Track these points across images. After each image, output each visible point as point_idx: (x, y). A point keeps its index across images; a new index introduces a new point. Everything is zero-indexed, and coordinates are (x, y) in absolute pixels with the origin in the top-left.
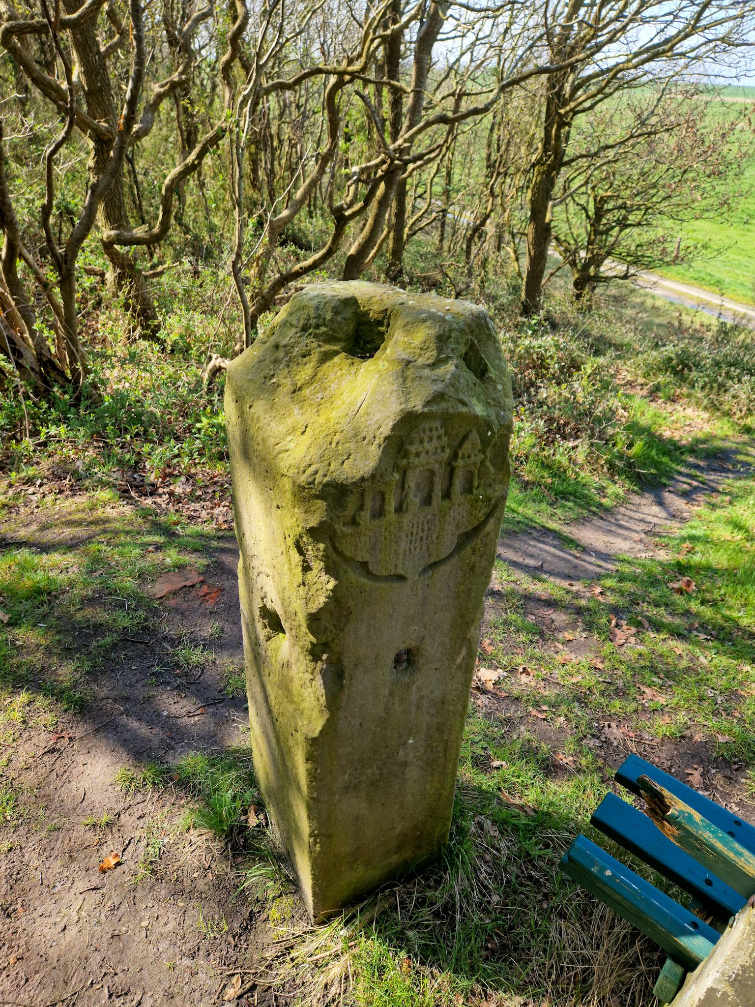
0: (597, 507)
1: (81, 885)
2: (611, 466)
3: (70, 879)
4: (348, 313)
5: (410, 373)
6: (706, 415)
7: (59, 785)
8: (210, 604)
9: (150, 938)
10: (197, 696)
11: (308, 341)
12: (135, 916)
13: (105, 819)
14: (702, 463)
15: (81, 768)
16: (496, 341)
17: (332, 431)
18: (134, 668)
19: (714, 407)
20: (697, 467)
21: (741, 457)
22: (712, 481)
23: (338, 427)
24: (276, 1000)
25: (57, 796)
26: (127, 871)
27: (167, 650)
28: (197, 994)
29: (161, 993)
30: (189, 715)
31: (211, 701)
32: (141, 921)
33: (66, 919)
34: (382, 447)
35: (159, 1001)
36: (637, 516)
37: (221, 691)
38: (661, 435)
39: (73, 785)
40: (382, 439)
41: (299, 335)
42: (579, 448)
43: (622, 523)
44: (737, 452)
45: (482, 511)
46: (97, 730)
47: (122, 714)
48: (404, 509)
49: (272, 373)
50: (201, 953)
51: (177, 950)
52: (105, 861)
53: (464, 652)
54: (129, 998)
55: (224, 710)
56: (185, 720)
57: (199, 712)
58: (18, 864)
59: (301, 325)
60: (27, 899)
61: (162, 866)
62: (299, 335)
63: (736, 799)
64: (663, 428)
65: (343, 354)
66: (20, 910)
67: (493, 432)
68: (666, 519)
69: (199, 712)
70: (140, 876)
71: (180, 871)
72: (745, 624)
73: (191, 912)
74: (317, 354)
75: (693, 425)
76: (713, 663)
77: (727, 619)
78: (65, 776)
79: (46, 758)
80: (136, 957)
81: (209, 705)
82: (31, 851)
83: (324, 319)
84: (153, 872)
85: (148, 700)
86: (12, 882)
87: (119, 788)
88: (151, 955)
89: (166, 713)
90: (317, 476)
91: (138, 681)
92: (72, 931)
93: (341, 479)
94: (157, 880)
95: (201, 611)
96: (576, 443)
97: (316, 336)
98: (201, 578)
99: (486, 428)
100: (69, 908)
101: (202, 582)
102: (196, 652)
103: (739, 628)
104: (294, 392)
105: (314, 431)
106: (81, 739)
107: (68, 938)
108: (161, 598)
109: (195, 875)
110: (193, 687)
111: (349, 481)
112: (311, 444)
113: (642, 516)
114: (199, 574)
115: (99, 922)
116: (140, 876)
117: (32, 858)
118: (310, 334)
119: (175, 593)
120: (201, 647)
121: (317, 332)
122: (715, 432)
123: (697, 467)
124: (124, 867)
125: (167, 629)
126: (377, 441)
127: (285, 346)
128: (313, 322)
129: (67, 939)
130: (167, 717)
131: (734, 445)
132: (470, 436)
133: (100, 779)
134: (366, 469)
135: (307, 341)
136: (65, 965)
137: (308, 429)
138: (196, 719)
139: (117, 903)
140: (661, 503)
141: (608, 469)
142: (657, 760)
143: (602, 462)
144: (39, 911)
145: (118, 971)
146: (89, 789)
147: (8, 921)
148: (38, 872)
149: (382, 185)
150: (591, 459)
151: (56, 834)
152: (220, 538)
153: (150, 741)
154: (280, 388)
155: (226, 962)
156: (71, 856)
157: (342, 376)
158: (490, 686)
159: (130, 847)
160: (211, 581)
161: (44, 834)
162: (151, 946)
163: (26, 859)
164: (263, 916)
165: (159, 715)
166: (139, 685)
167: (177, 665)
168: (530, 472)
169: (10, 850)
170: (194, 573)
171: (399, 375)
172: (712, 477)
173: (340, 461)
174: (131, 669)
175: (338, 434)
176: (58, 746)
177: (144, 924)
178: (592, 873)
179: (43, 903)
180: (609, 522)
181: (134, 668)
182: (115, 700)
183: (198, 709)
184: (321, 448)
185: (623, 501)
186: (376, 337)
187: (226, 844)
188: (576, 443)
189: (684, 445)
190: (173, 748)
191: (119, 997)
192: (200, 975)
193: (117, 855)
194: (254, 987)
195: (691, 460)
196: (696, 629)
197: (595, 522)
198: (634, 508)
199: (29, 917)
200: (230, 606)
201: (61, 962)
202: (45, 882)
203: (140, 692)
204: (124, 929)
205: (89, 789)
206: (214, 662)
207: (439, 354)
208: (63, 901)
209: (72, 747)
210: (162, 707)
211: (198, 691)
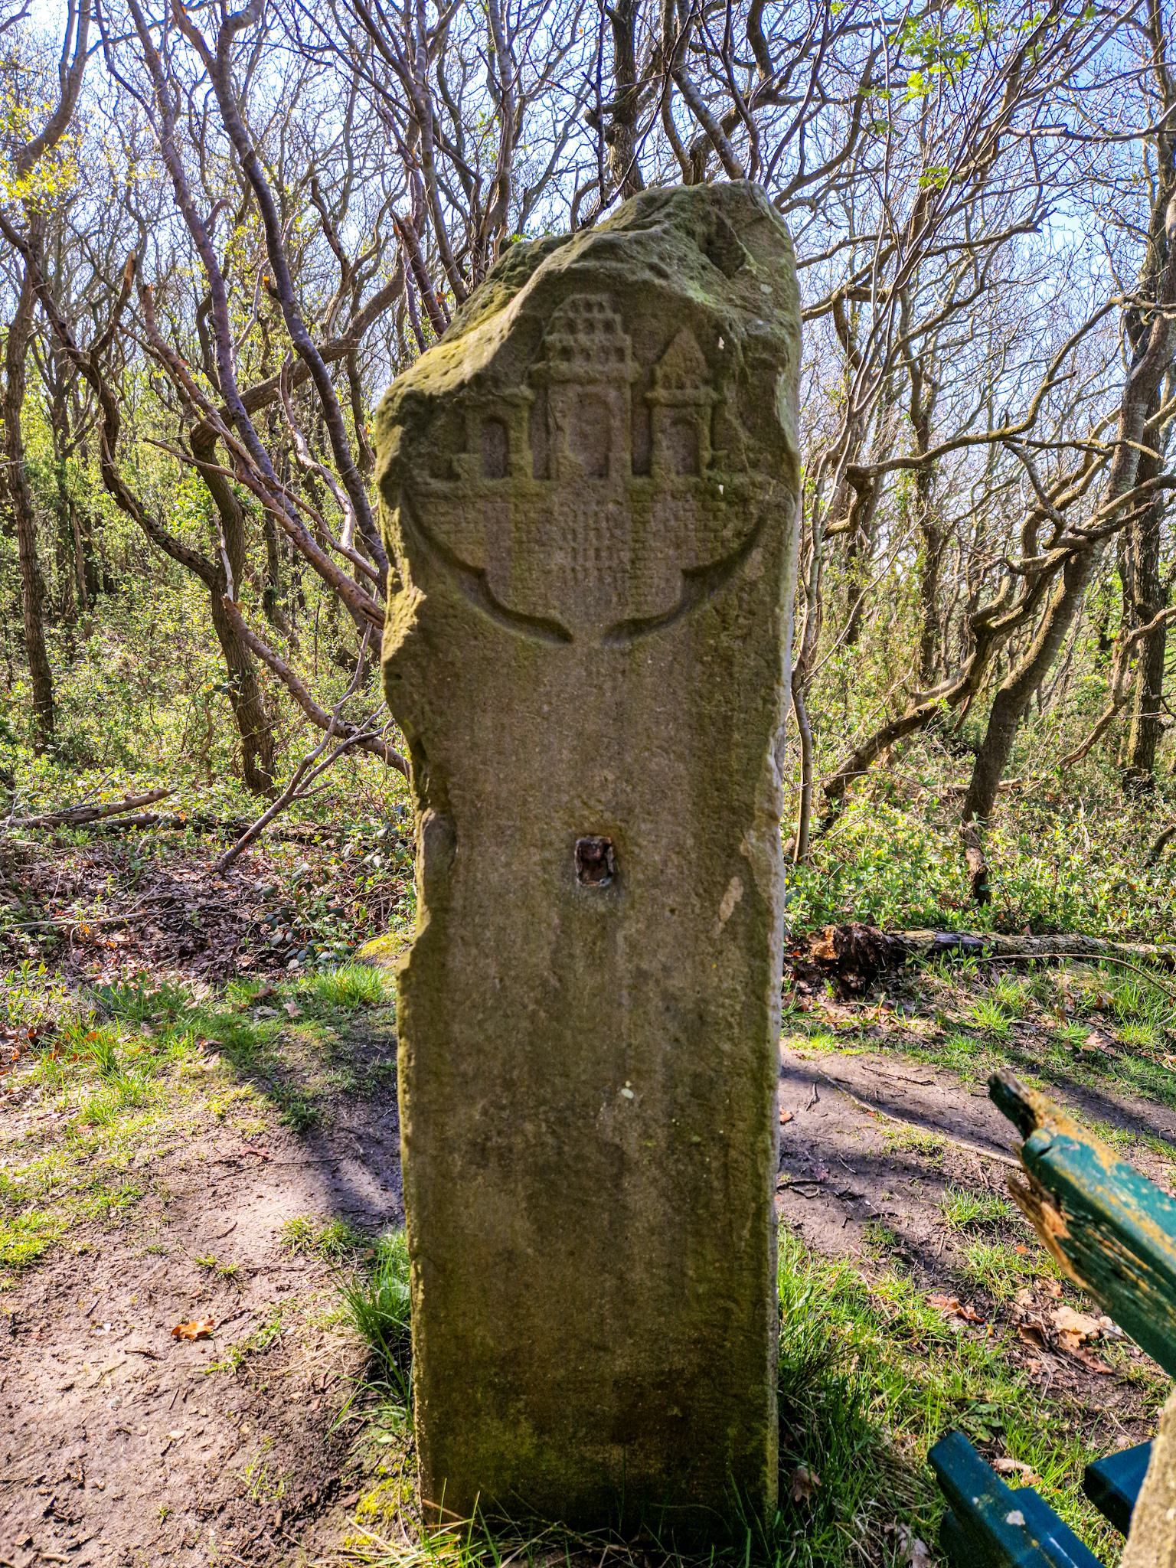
15: (252, 1199)
16: (782, 243)
26: (210, 1350)
35: (108, 1559)
45: (730, 525)
46: (308, 1164)
48: (553, 472)
51: (192, 1495)
53: (735, 892)
54: (71, 1531)
58: (78, 1276)
66: (35, 1335)
67: (729, 342)
70: (221, 1365)
73: (251, 1448)
79: (216, 1169)
92: (74, 1397)
99: (712, 332)
109: (295, 1396)
116: (221, 1365)
124: (208, 1345)
132: (677, 339)
136: (28, 1437)
144: (56, 1350)
147: (9, 1339)
149: (1059, 578)
158: (1071, 1343)
169: (83, 1253)
176: (242, 1162)
178: (972, 1506)
191: (59, 1521)
201: (26, 1431)
202: (94, 1317)
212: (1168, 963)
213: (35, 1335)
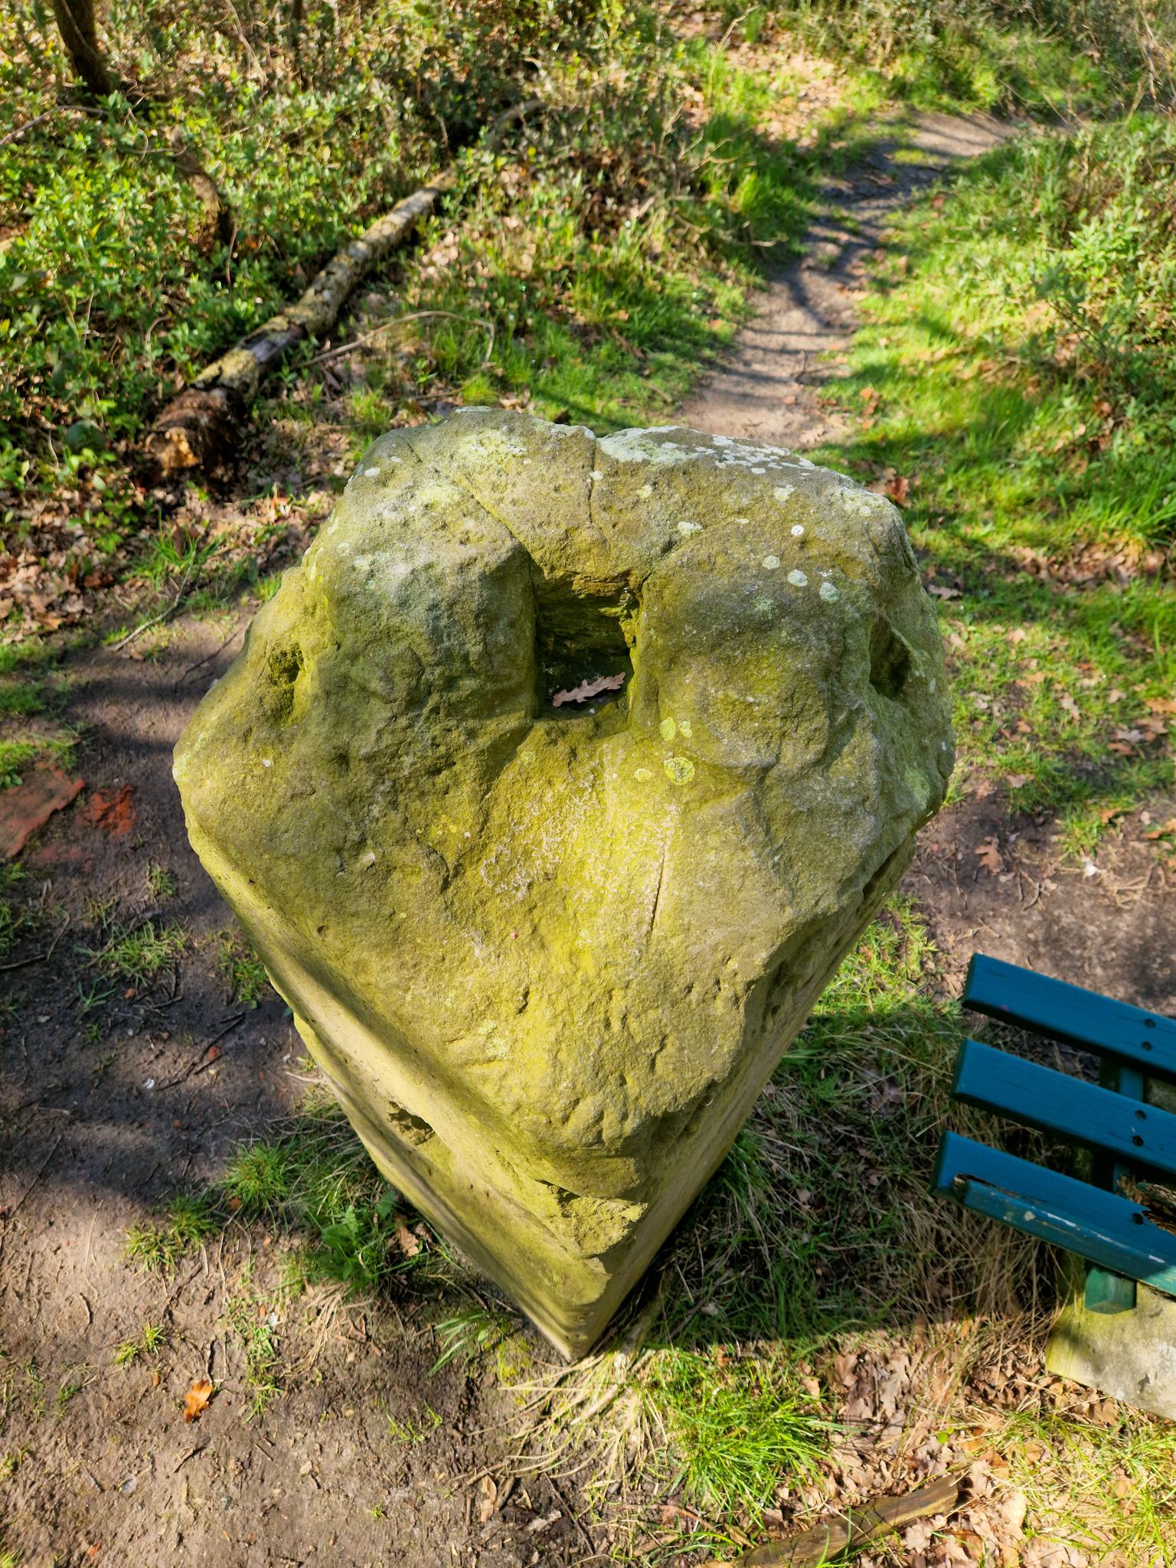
0: (712, 347)
1: (170, 1458)
2: (712, 243)
3: (146, 1457)
4: (515, 601)
5: (775, 799)
6: (828, 68)
7: (33, 1310)
8: (123, 832)
9: (325, 1486)
10: (191, 1028)
11: (436, 730)
12: (284, 1464)
13: (150, 1335)
14: (843, 186)
15: (53, 1260)
17: (599, 990)
18: (43, 1019)
19: (837, 47)
20: (836, 196)
21: (902, 157)
22: (867, 223)
23: (610, 974)
24: (556, 1486)
25: (40, 1332)
27: (89, 958)
28: (438, 1531)
29: (384, 1557)
30: (192, 1069)
31: (223, 1028)
32: (297, 1467)
33: (174, 1524)
34: (743, 1001)
36: (775, 342)
37: (231, 1000)
38: (766, 134)
39: (58, 1298)
40: (740, 989)
41: (403, 721)
42: (653, 219)
43: (757, 367)
44: (895, 145)
46: (43, 1176)
47: (71, 1123)
49: (354, 835)
50: (415, 1471)
51: (377, 1483)
52: (188, 1401)
55: (254, 1035)
56: (193, 1082)
57: (210, 1056)
59: (401, 692)
60: (91, 1527)
61: (289, 1366)
62: (403, 721)
63: (1050, 871)
64: (766, 115)
65: (540, 728)
68: (818, 335)
69: (210, 1056)
70: (259, 1398)
71: (322, 1362)
72: (996, 545)
74: (471, 761)
75: (812, 96)
76: (973, 643)
77: (972, 544)
78: (34, 1290)
80: (317, 1526)
81: (222, 1036)
82: (53, 1450)
83: (465, 658)
84: (278, 1382)
85: (106, 1073)
86: (50, 1516)
87: (144, 1267)
88: (341, 1510)
89: (150, 1084)
90: (605, 1123)
91: (66, 1044)
92: (196, 1536)
93: (664, 1102)
94: (291, 1391)
95: (112, 851)
96: (645, 208)
97: (454, 710)
98: (79, 783)
100: (169, 1503)
101: (85, 790)
102: (145, 940)
103: (988, 556)
104: (446, 885)
105: (551, 1003)
106: (22, 1206)
107: (195, 1550)
108: (20, 854)
110: (175, 1012)
111: (682, 1101)
112: (558, 1041)
113: (781, 339)
114: (69, 773)
115: (230, 1500)
116: (259, 1398)
117: (57, 1456)
118: (435, 710)
119: (42, 833)
120: (150, 925)
121: (454, 696)
122: (851, 107)
123: (836, 196)
124: (224, 1395)
125: (66, 915)
126: (726, 991)
127: (370, 758)
128: (433, 675)
129: (194, 1553)
130: (159, 1089)
131: (887, 130)
133: (101, 1264)
134: (718, 1063)
135: (427, 731)
137: (533, 999)
138: (212, 1072)
139: (244, 1456)
140: (801, 300)
141: (709, 252)
142: (935, 847)
143: (696, 238)
145: (300, 1559)
146: (90, 1291)
148: (85, 1475)
150: (678, 240)
151: (79, 1400)
152: (63, 658)
153: (151, 1151)
154: (396, 875)
155: (457, 1465)
156: (126, 1423)
157: (560, 800)
159: (217, 1359)
160: (99, 780)
161: (57, 1413)
162: (333, 1497)
163: (51, 1466)
164: (489, 1379)
165: (141, 1094)
166: (72, 1051)
167: (123, 980)
168: (585, 303)
169: (16, 1466)
170: (58, 774)
171: (751, 816)
172: (867, 215)
173: (644, 1061)
174: (38, 1024)
175: (617, 994)
177: (305, 1468)
179: (121, 1519)
180: (737, 373)
181: (43, 1019)
182: (45, 1102)
183: (206, 1051)
184: (587, 1048)
185: (744, 316)
186: (591, 625)
187: (380, 1294)
188: (645, 208)
189: (808, 149)
190: (199, 1148)
192: (429, 1502)
193: (203, 1383)
194: (517, 1483)
195: (825, 181)
196: (933, 582)
197: (717, 385)
198: (765, 326)
199: (112, 1553)
200: (164, 820)
202: (106, 1484)
203: (85, 1062)
204: (277, 1491)
205: (90, 1291)
206: (189, 947)
207: (832, 718)
208: (154, 1498)
209: (15, 1228)
210: (138, 1074)
211: (188, 1015)
212: (296, 12)
213: (90, 1550)
